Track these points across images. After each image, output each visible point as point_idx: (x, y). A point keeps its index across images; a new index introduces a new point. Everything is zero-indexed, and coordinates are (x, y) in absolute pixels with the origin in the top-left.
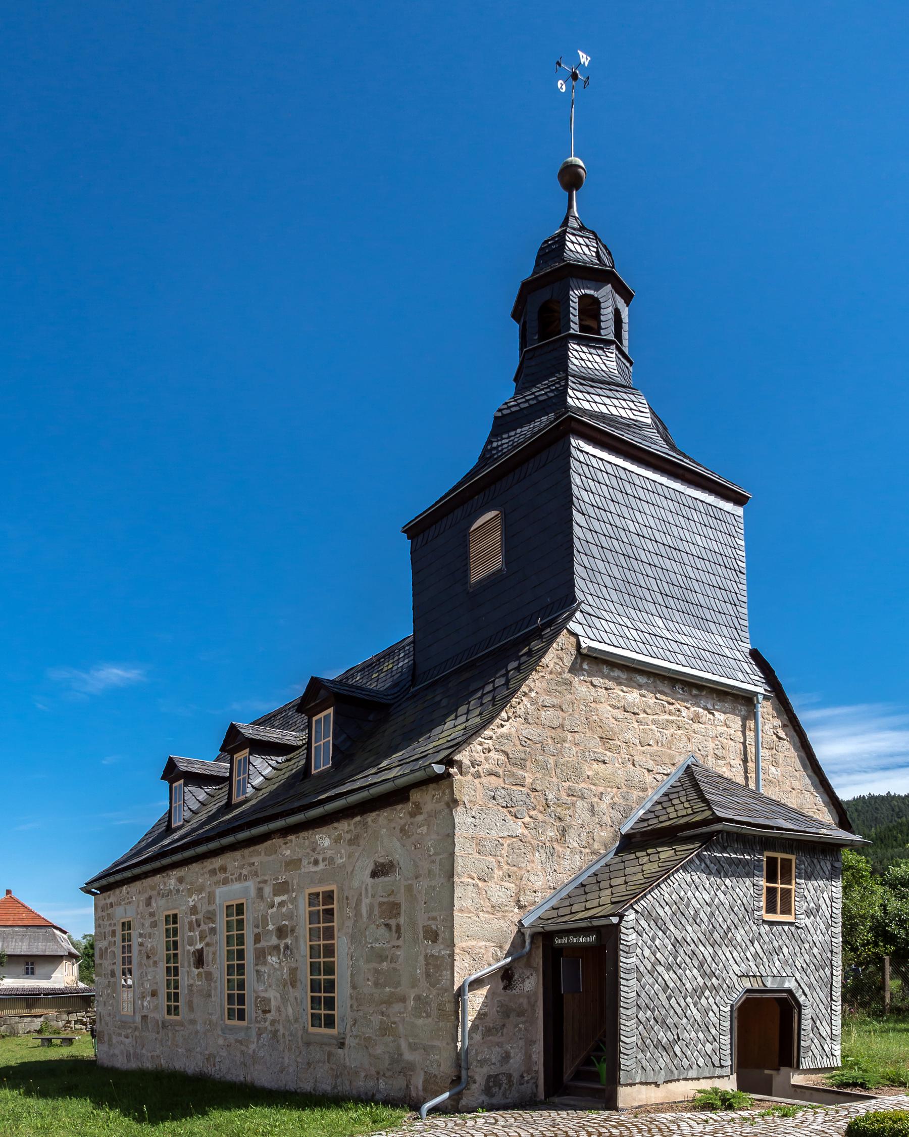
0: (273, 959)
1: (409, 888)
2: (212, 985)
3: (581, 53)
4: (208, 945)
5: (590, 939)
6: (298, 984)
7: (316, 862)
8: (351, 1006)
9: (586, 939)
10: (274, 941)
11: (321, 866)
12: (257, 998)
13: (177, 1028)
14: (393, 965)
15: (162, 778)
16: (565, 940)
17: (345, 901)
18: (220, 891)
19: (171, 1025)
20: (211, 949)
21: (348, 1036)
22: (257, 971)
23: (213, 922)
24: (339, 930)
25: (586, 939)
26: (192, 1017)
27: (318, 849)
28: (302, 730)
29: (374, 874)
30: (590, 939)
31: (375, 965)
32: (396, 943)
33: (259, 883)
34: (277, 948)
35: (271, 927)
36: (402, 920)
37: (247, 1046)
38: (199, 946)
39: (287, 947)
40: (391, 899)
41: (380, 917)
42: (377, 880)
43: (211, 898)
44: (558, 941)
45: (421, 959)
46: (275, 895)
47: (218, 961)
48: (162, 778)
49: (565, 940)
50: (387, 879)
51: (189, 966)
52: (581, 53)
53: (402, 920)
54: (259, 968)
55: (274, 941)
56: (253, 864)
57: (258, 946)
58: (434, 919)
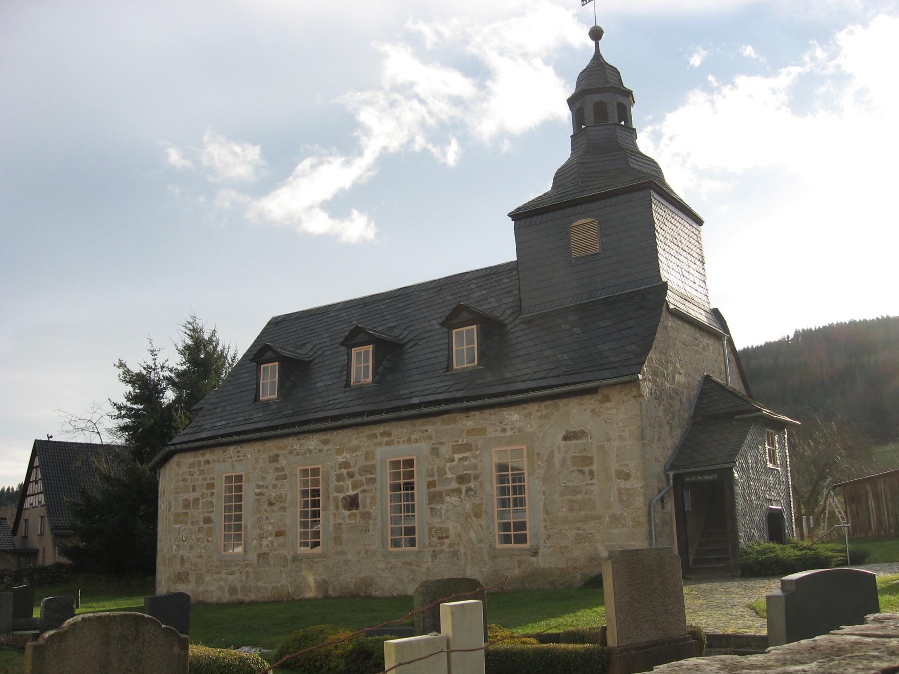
0: (453, 498)
1: (601, 448)
2: (371, 522)
3: (70, 562)
4: (364, 491)
5: (714, 477)
6: (484, 515)
7: (504, 430)
8: (545, 527)
9: (710, 477)
10: (454, 485)
11: (509, 433)
12: (431, 529)
13: (315, 560)
14: (588, 496)
15: (510, 215)
16: (693, 478)
17: (535, 456)
18: (379, 452)
19: (307, 558)
20: (368, 495)
21: (542, 547)
22: (431, 509)
23: (371, 473)
24: (529, 475)
25: (710, 477)
26: (340, 548)
27: (506, 421)
28: (64, 551)
29: (565, 438)
30: (714, 477)
31: (571, 497)
32: (592, 482)
33: (434, 444)
34: (459, 491)
35: (449, 475)
36: (594, 467)
37: (420, 567)
38: (351, 493)
39: (469, 489)
40: (584, 454)
41: (573, 466)
42: (568, 442)
43: (369, 455)
44: (687, 479)
45: (615, 491)
46: (454, 453)
47: (379, 503)
48: (510, 215)
49: (693, 478)
50: (579, 442)
51: (337, 508)
52: (70, 562)
53: (594, 467)
54: (433, 506)
55: (454, 485)
56: (427, 431)
57: (432, 490)
58: (627, 465)
